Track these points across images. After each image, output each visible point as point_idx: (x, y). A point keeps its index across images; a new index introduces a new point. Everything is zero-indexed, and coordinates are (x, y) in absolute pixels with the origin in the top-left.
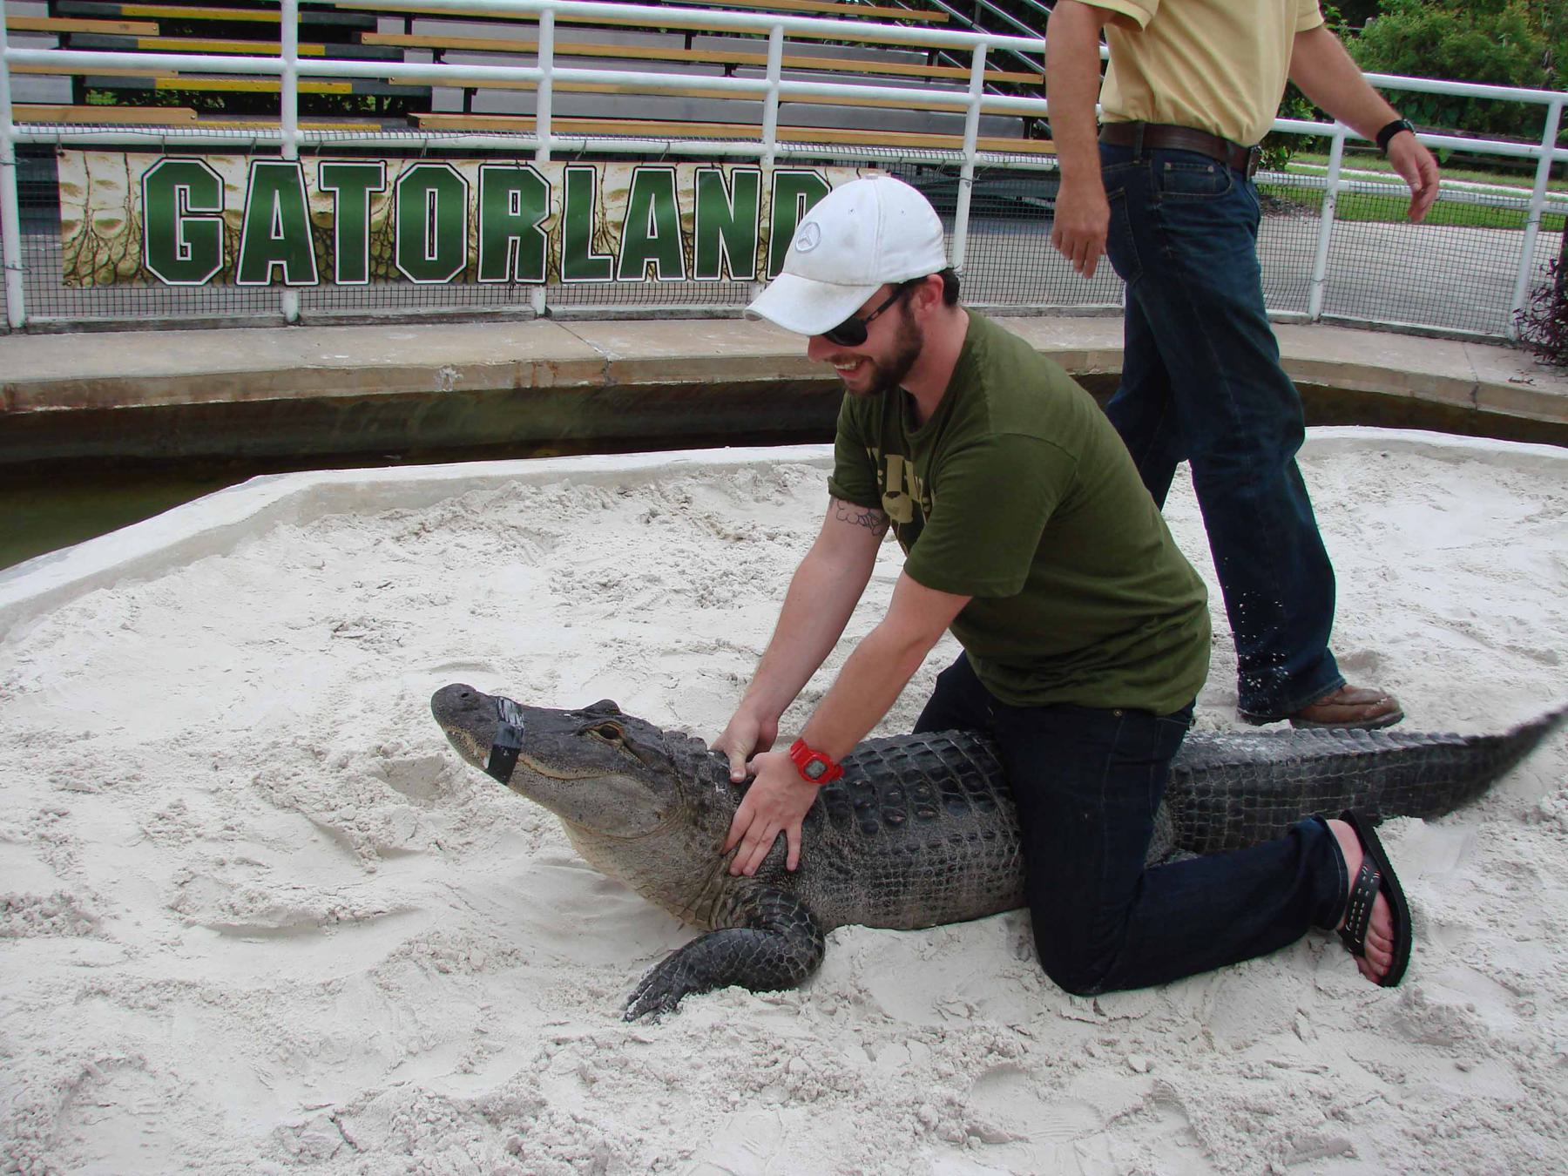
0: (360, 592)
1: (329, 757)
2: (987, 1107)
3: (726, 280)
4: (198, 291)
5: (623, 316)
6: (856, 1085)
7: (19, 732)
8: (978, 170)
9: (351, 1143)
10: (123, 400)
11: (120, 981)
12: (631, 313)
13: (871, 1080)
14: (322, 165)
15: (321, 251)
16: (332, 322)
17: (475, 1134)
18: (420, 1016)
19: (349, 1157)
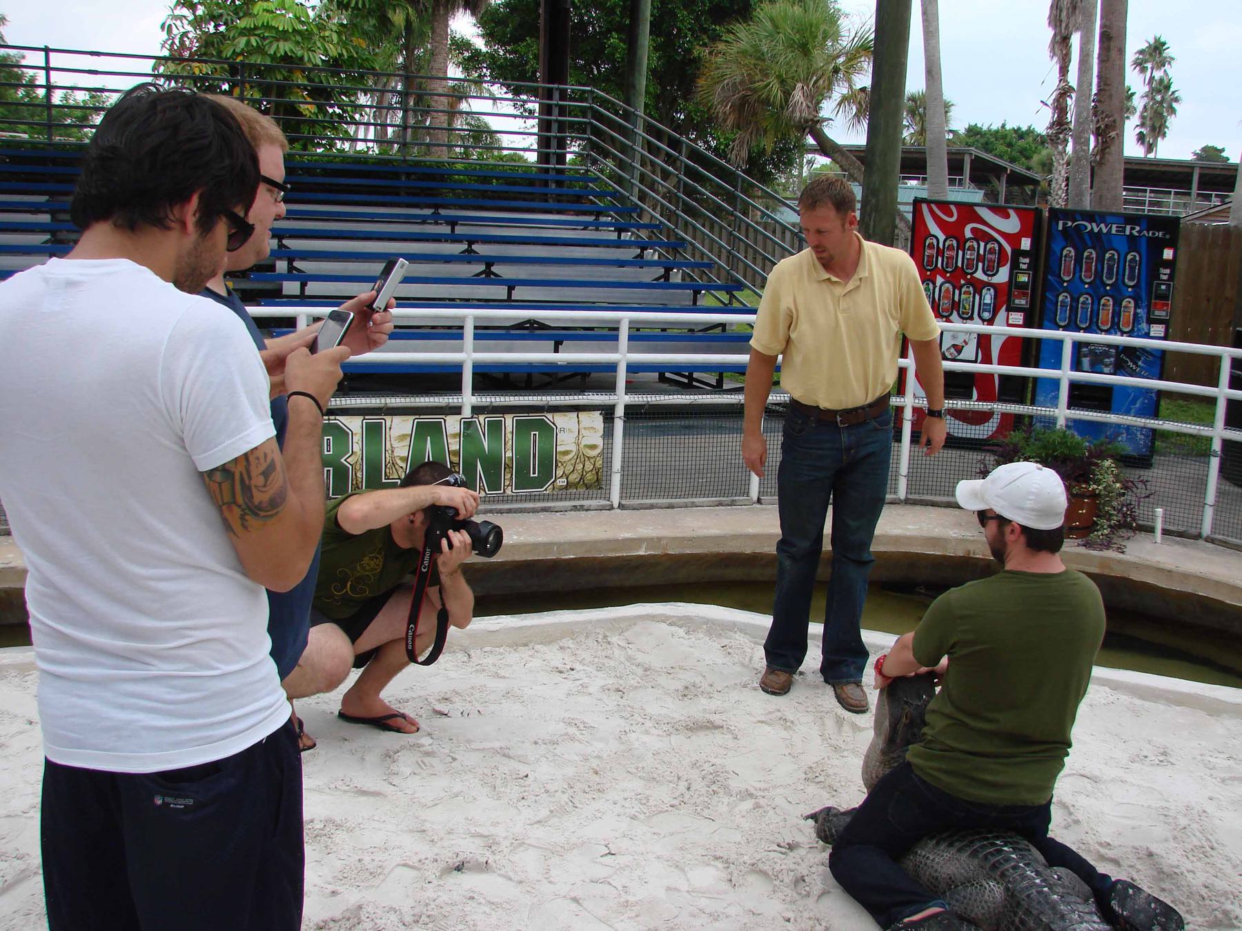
8: (627, 407)
14: (365, 421)
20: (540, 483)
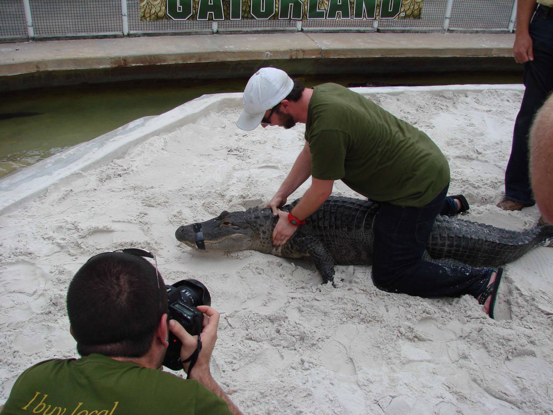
0: (236, 137)
1: (226, 197)
3: (365, 19)
4: (184, 22)
5: (328, 31)
6: (381, 319)
7: (132, 185)
9: (230, 325)
10: (160, 62)
11: (164, 270)
12: (331, 30)
13: (386, 318)
15: (226, 8)
16: (228, 33)
17: (266, 325)
18: (251, 287)
19: (229, 330)
20: (392, 15)
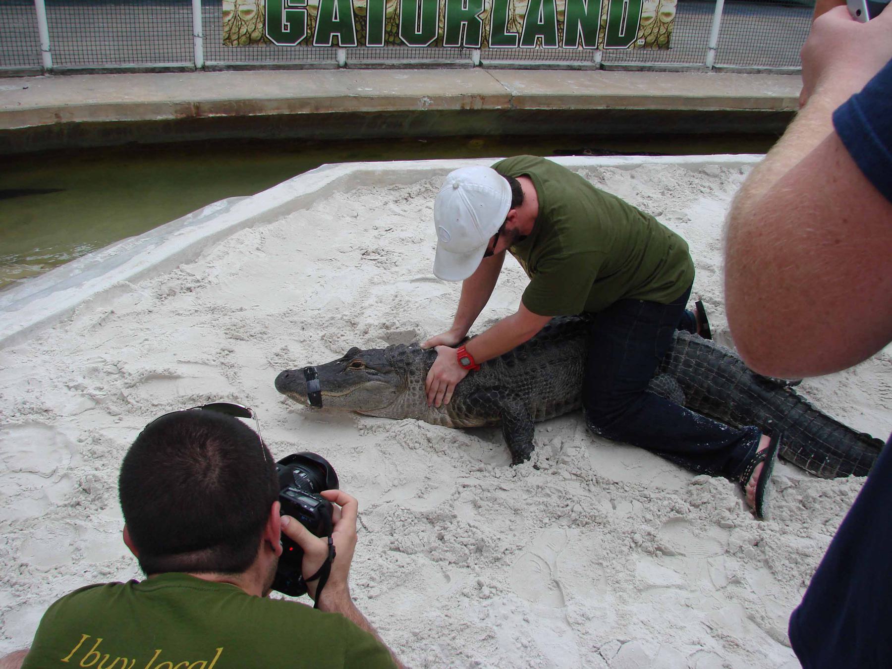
0: (376, 233)
2: (665, 538)
3: (580, 48)
4: (293, 49)
5: (522, 67)
6: (605, 521)
9: (365, 528)
15: (359, 28)
16: (363, 67)
17: (423, 528)
18: (399, 468)
